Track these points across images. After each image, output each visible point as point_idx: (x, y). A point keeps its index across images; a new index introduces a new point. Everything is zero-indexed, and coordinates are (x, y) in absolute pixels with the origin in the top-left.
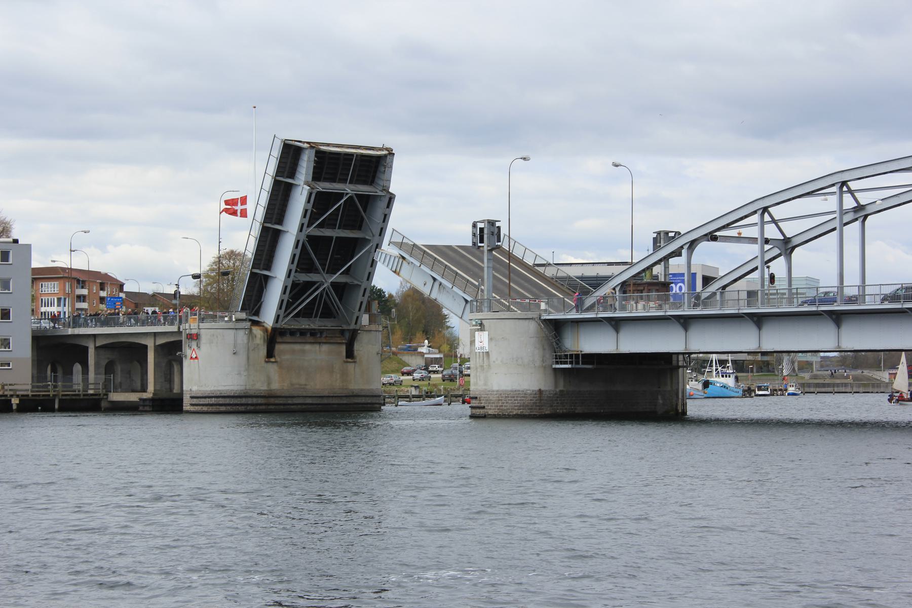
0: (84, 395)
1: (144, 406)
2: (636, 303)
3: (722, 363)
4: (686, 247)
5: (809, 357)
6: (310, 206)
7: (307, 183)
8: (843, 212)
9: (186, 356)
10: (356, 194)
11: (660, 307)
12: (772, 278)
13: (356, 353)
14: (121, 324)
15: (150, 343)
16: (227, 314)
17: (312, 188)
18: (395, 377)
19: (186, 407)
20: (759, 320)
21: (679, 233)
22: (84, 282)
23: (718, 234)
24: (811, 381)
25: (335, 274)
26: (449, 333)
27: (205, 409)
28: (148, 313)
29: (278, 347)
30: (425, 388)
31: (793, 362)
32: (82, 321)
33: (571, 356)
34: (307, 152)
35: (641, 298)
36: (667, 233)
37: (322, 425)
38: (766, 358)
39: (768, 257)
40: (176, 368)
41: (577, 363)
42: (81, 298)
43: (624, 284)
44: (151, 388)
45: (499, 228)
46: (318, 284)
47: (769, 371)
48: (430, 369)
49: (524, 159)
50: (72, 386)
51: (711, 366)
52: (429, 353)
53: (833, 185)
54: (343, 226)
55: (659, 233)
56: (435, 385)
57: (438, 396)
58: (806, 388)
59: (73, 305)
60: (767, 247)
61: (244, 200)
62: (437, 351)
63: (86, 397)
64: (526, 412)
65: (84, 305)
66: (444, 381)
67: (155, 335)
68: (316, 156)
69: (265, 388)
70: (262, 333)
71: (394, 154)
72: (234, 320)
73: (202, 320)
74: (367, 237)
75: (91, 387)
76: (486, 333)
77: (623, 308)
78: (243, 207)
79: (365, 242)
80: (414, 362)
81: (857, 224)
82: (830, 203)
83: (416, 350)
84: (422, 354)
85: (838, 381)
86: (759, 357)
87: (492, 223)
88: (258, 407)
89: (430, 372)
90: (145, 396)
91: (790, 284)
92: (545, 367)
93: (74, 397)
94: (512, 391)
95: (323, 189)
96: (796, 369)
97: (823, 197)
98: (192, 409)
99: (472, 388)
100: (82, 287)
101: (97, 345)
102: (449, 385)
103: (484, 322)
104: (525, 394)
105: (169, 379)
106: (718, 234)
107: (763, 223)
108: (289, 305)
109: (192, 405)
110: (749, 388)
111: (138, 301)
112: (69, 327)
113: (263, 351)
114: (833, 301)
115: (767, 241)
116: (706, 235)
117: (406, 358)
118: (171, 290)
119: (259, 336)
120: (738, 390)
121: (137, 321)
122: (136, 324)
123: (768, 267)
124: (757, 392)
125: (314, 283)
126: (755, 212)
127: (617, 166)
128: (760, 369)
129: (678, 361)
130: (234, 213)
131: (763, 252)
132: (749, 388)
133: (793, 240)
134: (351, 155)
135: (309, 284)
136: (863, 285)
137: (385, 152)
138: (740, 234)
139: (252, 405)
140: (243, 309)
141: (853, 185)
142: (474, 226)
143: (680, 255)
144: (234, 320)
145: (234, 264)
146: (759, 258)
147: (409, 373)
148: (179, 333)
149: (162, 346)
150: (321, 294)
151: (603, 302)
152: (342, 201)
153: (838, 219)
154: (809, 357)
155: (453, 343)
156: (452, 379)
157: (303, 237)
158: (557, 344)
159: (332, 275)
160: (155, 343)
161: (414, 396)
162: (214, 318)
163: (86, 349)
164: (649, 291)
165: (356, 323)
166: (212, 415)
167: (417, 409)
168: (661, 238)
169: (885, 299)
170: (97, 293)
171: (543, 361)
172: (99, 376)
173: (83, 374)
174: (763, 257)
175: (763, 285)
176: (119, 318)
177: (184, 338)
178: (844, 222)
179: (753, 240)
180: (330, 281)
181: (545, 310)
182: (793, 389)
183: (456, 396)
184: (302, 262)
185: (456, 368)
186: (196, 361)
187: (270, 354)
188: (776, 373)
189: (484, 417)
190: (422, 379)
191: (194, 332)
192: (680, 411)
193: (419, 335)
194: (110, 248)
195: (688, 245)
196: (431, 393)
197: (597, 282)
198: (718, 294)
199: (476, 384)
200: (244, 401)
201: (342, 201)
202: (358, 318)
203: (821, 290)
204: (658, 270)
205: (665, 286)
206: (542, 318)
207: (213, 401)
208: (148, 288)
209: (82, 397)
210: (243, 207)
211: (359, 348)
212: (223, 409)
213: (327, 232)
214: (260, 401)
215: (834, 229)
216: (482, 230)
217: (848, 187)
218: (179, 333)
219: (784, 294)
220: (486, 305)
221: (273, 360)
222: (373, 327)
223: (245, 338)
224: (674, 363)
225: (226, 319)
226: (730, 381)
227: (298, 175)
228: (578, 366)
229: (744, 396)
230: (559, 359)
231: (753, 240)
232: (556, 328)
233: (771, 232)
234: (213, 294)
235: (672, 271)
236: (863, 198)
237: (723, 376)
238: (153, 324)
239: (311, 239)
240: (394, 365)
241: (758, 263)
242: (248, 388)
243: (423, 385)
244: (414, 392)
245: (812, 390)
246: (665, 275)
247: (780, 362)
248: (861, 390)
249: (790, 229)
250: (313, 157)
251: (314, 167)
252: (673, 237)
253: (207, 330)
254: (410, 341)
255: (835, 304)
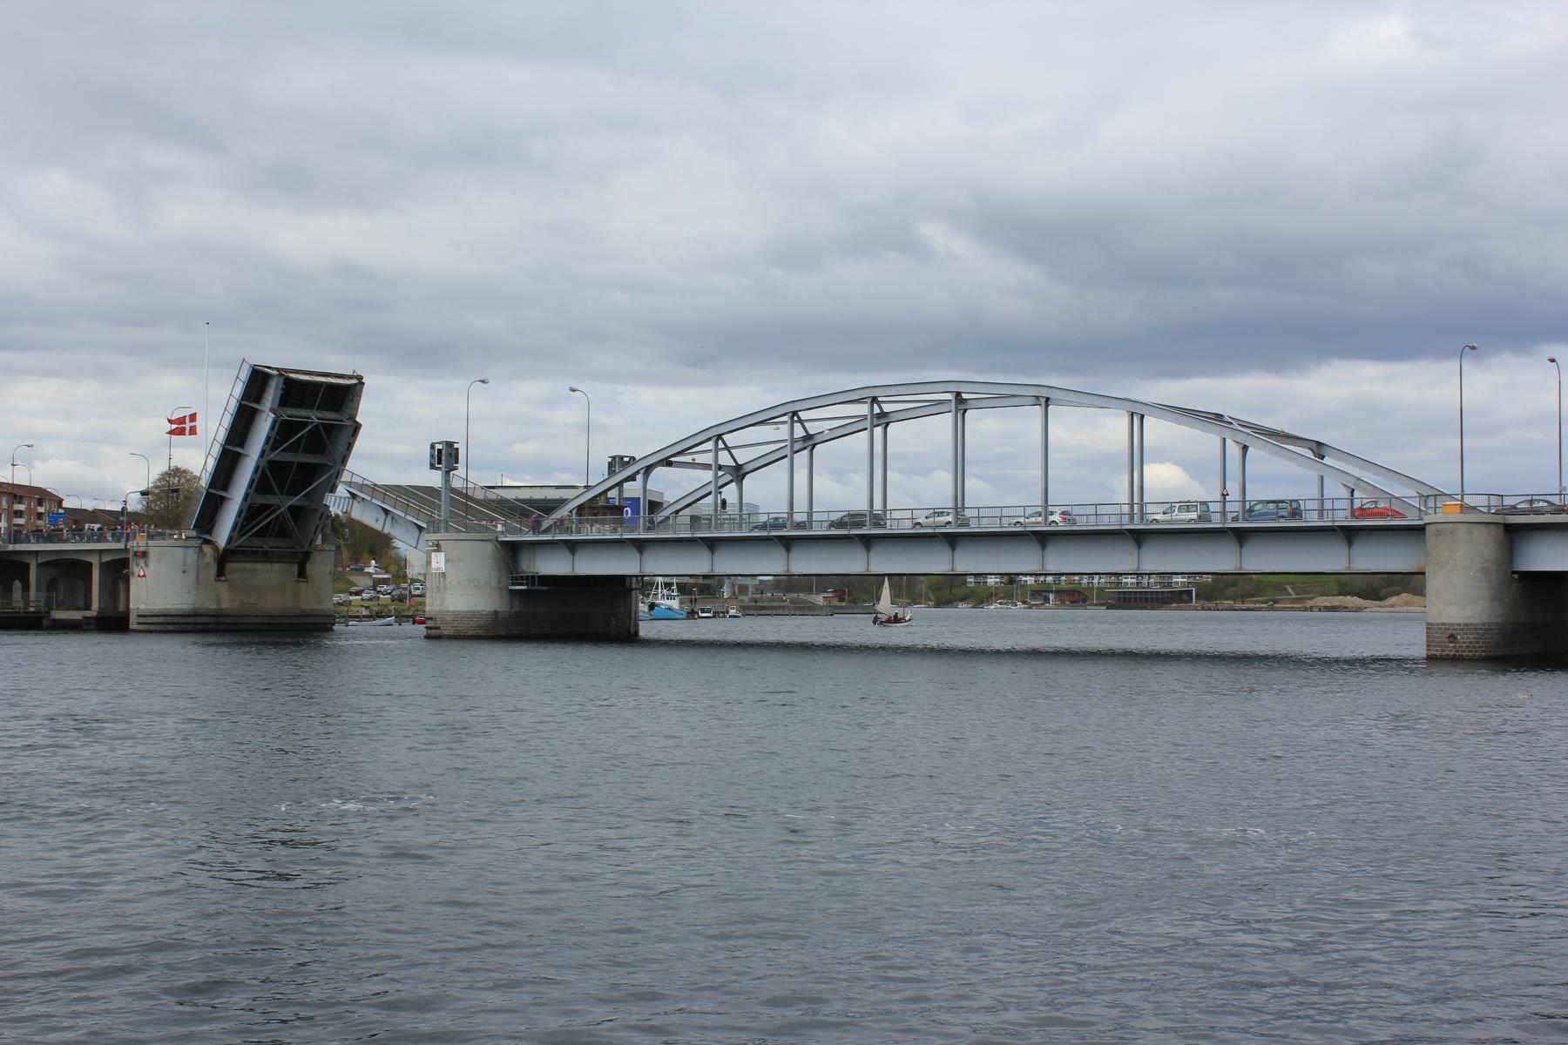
0: (25, 613)
1: (88, 624)
2: (591, 526)
3: (668, 585)
4: (642, 472)
5: (748, 581)
6: (274, 433)
7: (273, 410)
8: (793, 441)
9: (133, 574)
10: (323, 424)
11: (615, 531)
12: (724, 503)
13: (308, 573)
14: (65, 540)
15: (95, 560)
16: (177, 532)
17: (277, 416)
18: (343, 597)
19: (133, 626)
20: (712, 544)
21: (634, 458)
22: (21, 497)
23: (673, 459)
24: (751, 604)
25: (297, 495)
26: (395, 554)
27: (152, 627)
28: (93, 530)
29: (230, 566)
30: (376, 609)
31: (733, 586)
32: (23, 537)
33: (527, 577)
34: (276, 379)
35: (596, 521)
36: (622, 458)
37: (275, 645)
38: (708, 581)
39: (721, 482)
40: (122, 586)
41: (533, 584)
42: (19, 514)
43: (580, 507)
44: (95, 606)
45: (457, 449)
46: (275, 507)
47: (710, 594)
48: (379, 589)
49: (483, 382)
50: (11, 604)
51: (657, 588)
52: (376, 574)
53: (785, 415)
54: (306, 451)
55: (614, 458)
56: (386, 606)
57: (389, 617)
58: (746, 610)
59: (9, 521)
60: (720, 473)
61: (193, 417)
62: (383, 571)
63: (26, 615)
64: (482, 633)
65: (21, 521)
66: (393, 601)
67: (101, 552)
68: (284, 383)
69: (214, 607)
70: (212, 551)
71: (364, 383)
72: (184, 537)
73: (151, 537)
74: (330, 464)
75: (32, 604)
76: (443, 554)
77: (579, 531)
78: (193, 424)
79: (323, 468)
80: (362, 582)
81: (806, 452)
82: (782, 432)
83: (362, 570)
84: (370, 574)
85: (776, 604)
86: (700, 581)
87: (450, 445)
88: (207, 626)
89: (378, 592)
90: (89, 614)
91: (741, 510)
92: (501, 589)
93: (13, 615)
94: (467, 612)
95: (288, 416)
96: (736, 591)
97: (775, 426)
98: (139, 627)
99: (428, 608)
100: (19, 503)
101: (39, 562)
102: (400, 606)
103: (441, 542)
104: (480, 614)
105: (115, 599)
106: (673, 459)
107: (717, 450)
108: (243, 527)
109: (139, 623)
110: (693, 610)
111: (79, 519)
112: (10, 543)
113: (213, 570)
114: (783, 526)
115: (720, 468)
116: (662, 460)
117: (354, 578)
118: (117, 507)
119: (209, 554)
120: (682, 612)
121: (82, 538)
122: (80, 541)
123: (720, 493)
124: (700, 614)
125: (271, 506)
126: (709, 439)
127: (574, 391)
128: (701, 592)
129: (631, 583)
130: (181, 432)
131: (717, 478)
132: (693, 610)
133: (745, 466)
134: (318, 385)
135: (265, 507)
136: (810, 514)
137: (354, 381)
138: (694, 460)
139: (201, 624)
140: (195, 527)
141: (803, 415)
142: (432, 447)
143: (634, 480)
144: (184, 537)
145: (178, 481)
146: (713, 482)
147: (357, 593)
148: (126, 550)
149: (107, 563)
150: (278, 516)
151: (560, 525)
152: (307, 429)
153: (789, 447)
154: (748, 581)
155: (401, 563)
156: (401, 599)
157: (263, 463)
158: (514, 566)
159: (291, 497)
160: (100, 559)
161: (365, 616)
162: (162, 535)
163: (27, 566)
164: (604, 514)
165: (310, 546)
166: (157, 635)
167: (372, 629)
168: (617, 463)
169: (833, 525)
170: (35, 508)
171: (499, 582)
172: (41, 593)
173: (23, 591)
174: (716, 483)
175: (716, 510)
176: (63, 534)
177: (131, 555)
178: (795, 449)
179: (707, 467)
180: (287, 505)
181: (502, 532)
182: (734, 611)
183: (407, 617)
184: (260, 484)
185: (405, 589)
186: (144, 579)
187: (220, 573)
188: (717, 595)
189: (440, 637)
190: (371, 599)
191: (142, 549)
192: (632, 632)
193: (365, 555)
194: (37, 463)
195: (643, 470)
196: (381, 613)
197: (549, 507)
198: (671, 518)
199: (432, 605)
200: (192, 620)
201: (307, 429)
202: (312, 540)
203: (771, 516)
204: (613, 494)
205: (619, 510)
206: (499, 539)
207: (161, 620)
208: (89, 505)
209: (22, 615)
210: (193, 424)
211: (311, 568)
212: (171, 627)
213: (290, 457)
214: (210, 620)
215: (786, 456)
216: (440, 451)
217: (799, 417)
218: (126, 550)
219: (734, 519)
220: (443, 526)
221: (223, 579)
222: (326, 547)
223: (195, 556)
224: (628, 585)
225: (175, 537)
226: (675, 604)
227: (263, 401)
228: (533, 588)
229: (688, 618)
230: (516, 580)
231: (707, 467)
232: (512, 551)
233: (724, 459)
234: (157, 511)
235: (626, 495)
236: (813, 428)
237: (668, 599)
238: (98, 541)
239: (272, 464)
240: (342, 585)
241: (712, 488)
242: (197, 606)
243: (373, 606)
244: (365, 612)
245: (751, 612)
246: (620, 499)
247: (721, 585)
248: (798, 613)
249: (742, 457)
250: (281, 385)
251: (282, 394)
252: (628, 463)
253: (155, 548)
254: (357, 561)
255: (785, 530)
